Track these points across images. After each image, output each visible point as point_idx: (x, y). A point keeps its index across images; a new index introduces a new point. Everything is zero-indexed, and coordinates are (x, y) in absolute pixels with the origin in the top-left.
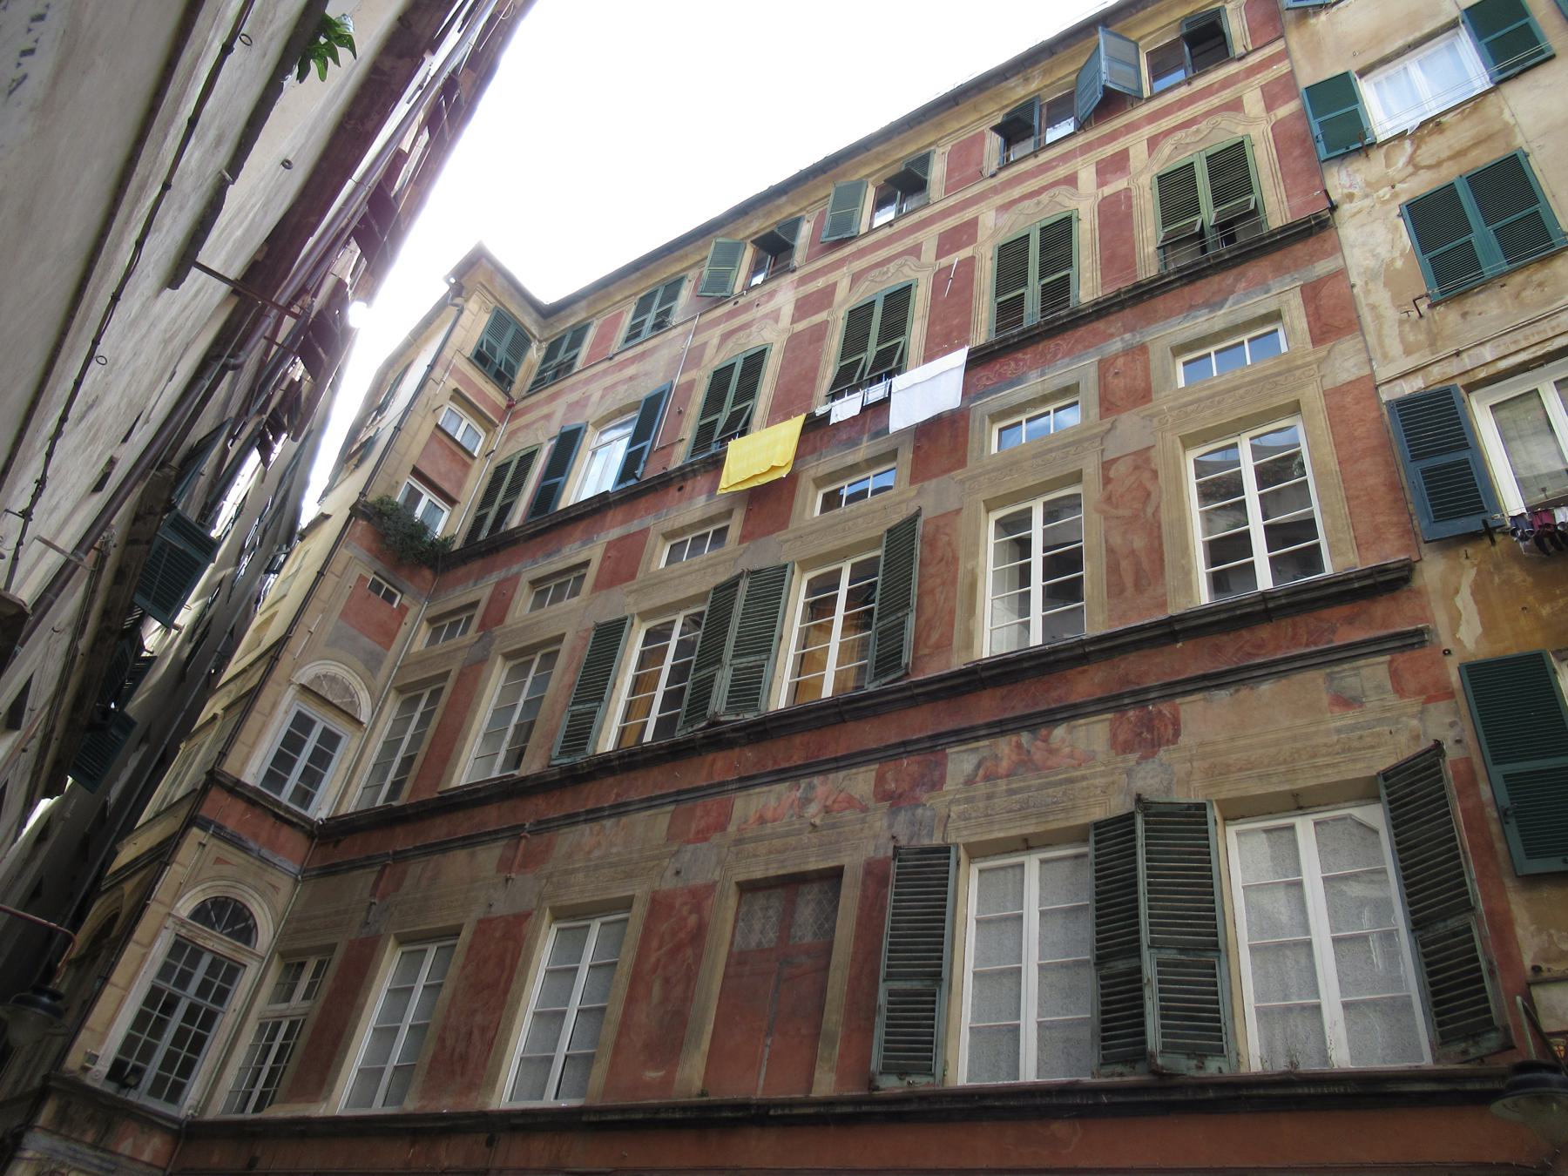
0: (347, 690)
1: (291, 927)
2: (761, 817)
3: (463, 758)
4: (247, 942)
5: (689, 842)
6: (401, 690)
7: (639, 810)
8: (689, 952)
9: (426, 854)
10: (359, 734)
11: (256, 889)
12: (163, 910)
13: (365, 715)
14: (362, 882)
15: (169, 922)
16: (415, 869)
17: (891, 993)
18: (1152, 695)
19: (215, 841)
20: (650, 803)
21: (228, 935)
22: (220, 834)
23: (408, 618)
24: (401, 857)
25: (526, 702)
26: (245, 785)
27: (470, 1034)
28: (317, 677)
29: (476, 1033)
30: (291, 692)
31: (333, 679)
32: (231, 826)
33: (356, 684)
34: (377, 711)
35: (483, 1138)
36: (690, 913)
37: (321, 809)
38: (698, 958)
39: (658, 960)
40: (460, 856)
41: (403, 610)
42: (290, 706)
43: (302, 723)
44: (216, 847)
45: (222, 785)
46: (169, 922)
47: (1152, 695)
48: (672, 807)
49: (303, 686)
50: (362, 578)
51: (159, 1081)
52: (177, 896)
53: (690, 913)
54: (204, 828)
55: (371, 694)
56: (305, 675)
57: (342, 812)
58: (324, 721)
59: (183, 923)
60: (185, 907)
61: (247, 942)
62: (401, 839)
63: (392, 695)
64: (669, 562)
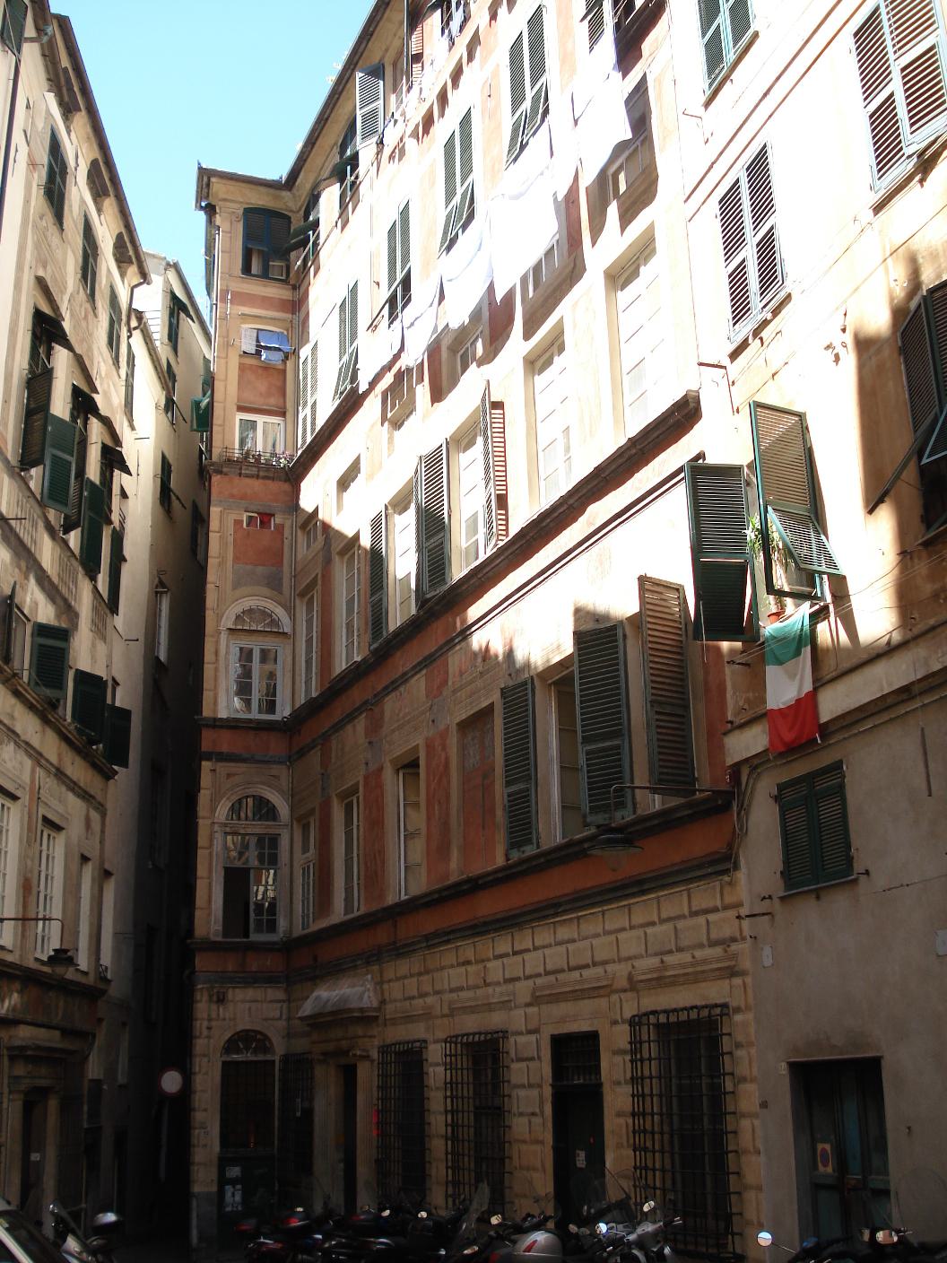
0: (264, 614)
2: (460, 671)
3: (337, 650)
6: (302, 595)
7: (413, 676)
9: (336, 731)
11: (263, 783)
12: (209, 821)
14: (315, 757)
15: (216, 828)
17: (588, 753)
18: (457, 641)
19: (221, 764)
21: (260, 819)
23: (287, 533)
25: (306, 641)
27: (375, 855)
28: (238, 617)
30: (223, 637)
31: (250, 611)
32: (225, 749)
33: (270, 605)
34: (293, 618)
37: (284, 711)
41: (280, 528)
45: (207, 726)
46: (216, 828)
47: (457, 641)
48: (424, 672)
50: (238, 523)
51: (259, 923)
52: (213, 810)
54: (209, 759)
56: (228, 622)
57: (297, 706)
58: (256, 645)
59: (225, 825)
60: (222, 811)
63: (298, 602)
64: (307, 549)
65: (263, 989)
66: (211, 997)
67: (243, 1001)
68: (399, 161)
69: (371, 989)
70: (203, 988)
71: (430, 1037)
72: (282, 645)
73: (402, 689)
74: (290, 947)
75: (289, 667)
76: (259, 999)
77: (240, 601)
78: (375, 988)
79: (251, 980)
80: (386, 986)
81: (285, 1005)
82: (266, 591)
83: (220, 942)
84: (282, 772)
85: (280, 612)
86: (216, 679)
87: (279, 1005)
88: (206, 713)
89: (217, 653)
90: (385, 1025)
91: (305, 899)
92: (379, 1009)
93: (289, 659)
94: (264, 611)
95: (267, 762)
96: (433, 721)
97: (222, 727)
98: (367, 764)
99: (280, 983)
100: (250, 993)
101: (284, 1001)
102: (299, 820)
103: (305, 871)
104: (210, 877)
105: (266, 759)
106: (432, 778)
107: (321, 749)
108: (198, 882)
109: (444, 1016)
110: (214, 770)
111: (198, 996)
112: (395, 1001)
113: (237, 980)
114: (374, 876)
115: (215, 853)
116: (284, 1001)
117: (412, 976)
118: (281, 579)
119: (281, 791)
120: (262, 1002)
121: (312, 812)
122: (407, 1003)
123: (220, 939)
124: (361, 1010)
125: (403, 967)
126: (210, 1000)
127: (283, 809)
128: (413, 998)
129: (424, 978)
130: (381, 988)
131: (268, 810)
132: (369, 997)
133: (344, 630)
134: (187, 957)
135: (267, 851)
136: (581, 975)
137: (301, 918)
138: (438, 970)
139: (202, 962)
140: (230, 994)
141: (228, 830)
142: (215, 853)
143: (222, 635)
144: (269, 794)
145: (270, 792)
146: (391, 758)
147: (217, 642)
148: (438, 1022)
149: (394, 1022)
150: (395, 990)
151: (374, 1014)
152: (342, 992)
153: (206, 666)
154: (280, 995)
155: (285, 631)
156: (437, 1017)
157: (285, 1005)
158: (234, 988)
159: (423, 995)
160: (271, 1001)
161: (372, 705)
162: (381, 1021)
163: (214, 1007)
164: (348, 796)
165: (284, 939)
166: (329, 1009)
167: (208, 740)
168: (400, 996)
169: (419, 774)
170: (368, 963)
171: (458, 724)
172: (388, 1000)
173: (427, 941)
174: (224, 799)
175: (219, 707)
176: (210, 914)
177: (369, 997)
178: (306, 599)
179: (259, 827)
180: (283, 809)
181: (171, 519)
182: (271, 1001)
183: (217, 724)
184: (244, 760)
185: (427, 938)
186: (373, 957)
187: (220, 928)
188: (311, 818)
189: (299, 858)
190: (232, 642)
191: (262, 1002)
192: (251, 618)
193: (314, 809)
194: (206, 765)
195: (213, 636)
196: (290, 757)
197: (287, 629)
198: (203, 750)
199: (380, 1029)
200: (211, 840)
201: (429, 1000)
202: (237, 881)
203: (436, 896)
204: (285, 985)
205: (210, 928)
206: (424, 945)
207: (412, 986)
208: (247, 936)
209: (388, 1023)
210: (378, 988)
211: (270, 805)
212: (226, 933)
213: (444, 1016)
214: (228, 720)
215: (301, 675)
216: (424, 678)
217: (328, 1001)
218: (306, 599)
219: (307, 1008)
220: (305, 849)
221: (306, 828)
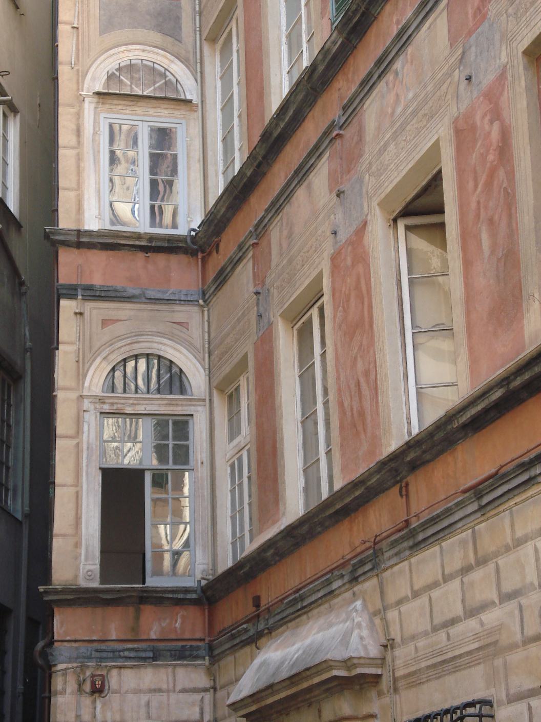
0: (154, 72)
1: (212, 354)
4: (182, 391)
5: (470, 34)
6: (212, 39)
8: (501, 173)
9: (277, 212)
10: (194, 115)
12: (74, 395)
13: (190, 91)
15: (86, 404)
16: (275, 234)
20: (302, 173)
22: (93, 294)
24: (261, 229)
26: (90, 233)
27: (358, 384)
28: (110, 77)
29: (362, 380)
30: (89, 107)
31: (131, 68)
32: (98, 280)
35: (396, 489)
36: (492, 122)
38: (511, 175)
39: (479, 203)
40: (301, 194)
42: (96, 122)
43: (111, 126)
44: (95, 310)
45: (66, 244)
46: (86, 404)
49: (99, 94)
52: (81, 375)
53: (492, 122)
54: (72, 297)
55: (185, 61)
59: (102, 400)
60: (95, 381)
61: (182, 391)
62: (258, 205)
65: (170, 670)
66: (80, 685)
67: (137, 691)
68: (286, 660)
69: (364, 624)
70: (66, 669)
71: (495, 693)
72: (183, 121)
73: (398, 65)
74: (211, 595)
75: (197, 154)
76: (164, 687)
77: (112, 52)
78: (371, 621)
79: (155, 654)
80: (392, 615)
81: (208, 697)
82: (156, 37)
83: (95, 590)
84: (192, 316)
85: (178, 70)
86: (79, 171)
87: (197, 697)
88: (66, 222)
89: (78, 132)
90: (396, 690)
91: (237, 512)
92: (382, 661)
93: (197, 144)
94: (154, 69)
95: (169, 301)
96: (469, 79)
97: (90, 246)
98: (335, 233)
99: (196, 657)
100: (149, 676)
101: (205, 690)
102: (221, 390)
103: (235, 468)
104: (77, 483)
105: (166, 296)
106: (471, 185)
107: (253, 257)
108: (58, 491)
109: (527, 641)
110: (81, 314)
111: (58, 683)
112: (413, 638)
113: (127, 654)
114: (357, 419)
115: (85, 446)
116: (205, 690)
117: (446, 579)
118: (178, 19)
119: (190, 346)
120: (168, 691)
121: (242, 365)
122: (442, 635)
123: (96, 584)
124: (348, 663)
125: (428, 563)
126: (80, 689)
127: (197, 377)
128: (453, 622)
129: (477, 575)
130: (384, 619)
131: (171, 377)
132: (362, 638)
133: (285, 48)
134: (40, 624)
135: (171, 443)
136: (482, 624)
137: (230, 547)
138: (508, 549)
139: (66, 625)
140: (114, 678)
141: (106, 408)
142: (85, 446)
143: (86, 105)
144: (171, 351)
145: (175, 349)
146: (378, 200)
147: (79, 115)
148: (515, 657)
149: (415, 679)
150: (413, 617)
151: (373, 671)
152: (308, 641)
153: (61, 152)
154: (200, 678)
155: (189, 97)
156: (513, 647)
157: (208, 697)
158: (120, 667)
159: (472, 612)
160: (184, 691)
161: (341, 128)
162: (385, 683)
163: (87, 701)
164: (301, 318)
165: (203, 583)
166: (284, 674)
167: (70, 266)
168: (425, 625)
169: (442, 226)
170: (354, 580)
171: (526, 53)
172: (398, 639)
173: (479, 497)
174: (99, 360)
175: (86, 215)
176: (77, 545)
177: (362, 638)
178: (219, 46)
179: (160, 405)
180: (197, 377)
181: (17, 7)
182: (184, 691)
183: (83, 241)
184: (129, 299)
185: (477, 491)
186: (364, 565)
187: (96, 567)
188: (244, 377)
189: (225, 449)
190: (102, 115)
191: (168, 691)
192: (132, 78)
193: (244, 361)
194: (67, 306)
195: (72, 106)
196: (204, 294)
197: (196, 99)
198: (61, 282)
199: (386, 700)
200: (79, 422)
201: (491, 617)
202: (123, 493)
203: (498, 394)
204: (207, 662)
205: (78, 568)
206: (474, 507)
207: (449, 599)
208: (144, 583)
209: (400, 684)
210: (377, 621)
211: (174, 370)
212: (105, 576)
213: (527, 641)
214: (100, 233)
215: (216, 164)
216: (445, 14)
217: (282, 663)
218: (219, 46)
219: (246, 686)
220: (234, 432)
221: (233, 399)
